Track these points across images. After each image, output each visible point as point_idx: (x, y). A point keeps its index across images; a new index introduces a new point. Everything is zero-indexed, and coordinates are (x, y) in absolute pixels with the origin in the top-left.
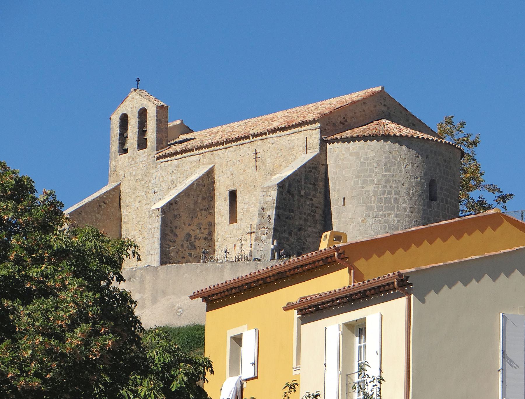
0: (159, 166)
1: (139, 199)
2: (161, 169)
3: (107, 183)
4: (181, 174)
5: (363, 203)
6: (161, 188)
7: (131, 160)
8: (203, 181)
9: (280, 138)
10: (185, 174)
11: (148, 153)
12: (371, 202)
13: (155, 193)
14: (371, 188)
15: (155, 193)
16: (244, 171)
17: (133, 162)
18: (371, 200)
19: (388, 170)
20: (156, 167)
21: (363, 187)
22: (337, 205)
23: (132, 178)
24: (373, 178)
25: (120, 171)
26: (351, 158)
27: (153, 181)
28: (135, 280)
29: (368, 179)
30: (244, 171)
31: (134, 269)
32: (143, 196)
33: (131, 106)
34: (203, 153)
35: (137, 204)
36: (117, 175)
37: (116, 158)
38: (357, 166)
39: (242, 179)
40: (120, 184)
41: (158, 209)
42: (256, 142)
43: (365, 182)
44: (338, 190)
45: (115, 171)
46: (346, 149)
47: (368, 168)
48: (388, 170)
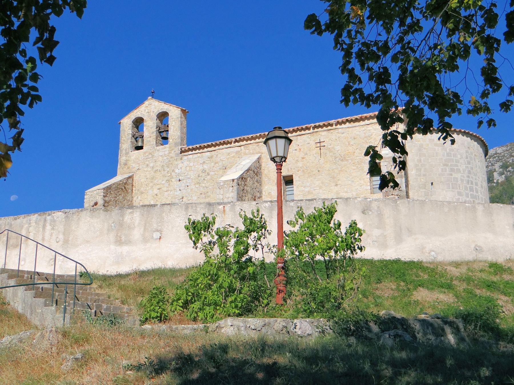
0: (185, 158)
1: (158, 187)
2: (189, 160)
3: (115, 174)
4: (216, 163)
5: (453, 188)
6: (189, 177)
7: (147, 154)
8: (129, 201)
9: (351, 129)
10: (220, 164)
11: (170, 148)
12: (460, 189)
13: (180, 180)
14: (458, 176)
15: (180, 180)
16: (303, 158)
17: (150, 156)
18: (459, 186)
19: (469, 163)
20: (181, 159)
21: (451, 175)
22: (425, 189)
23: (149, 169)
24: (459, 167)
25: (134, 165)
26: (437, 148)
27: (177, 171)
28: (370, 213)
29: (455, 168)
30: (303, 158)
31: (369, 200)
32: (163, 184)
33: (147, 111)
34: (246, 145)
35: (156, 191)
36: (128, 168)
37: (127, 154)
38: (443, 156)
39: (301, 165)
40: (133, 175)
41: (233, 180)
42: (321, 133)
43: (452, 170)
44: (424, 175)
45: (125, 164)
46: (430, 140)
47: (454, 158)
48: (469, 163)
